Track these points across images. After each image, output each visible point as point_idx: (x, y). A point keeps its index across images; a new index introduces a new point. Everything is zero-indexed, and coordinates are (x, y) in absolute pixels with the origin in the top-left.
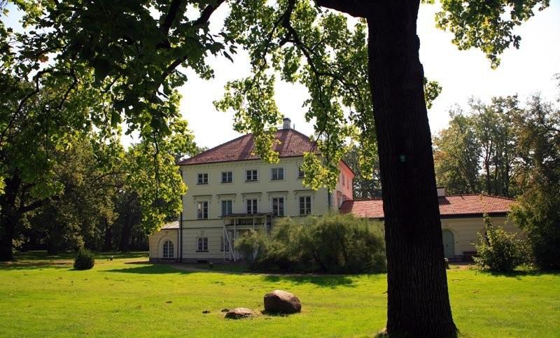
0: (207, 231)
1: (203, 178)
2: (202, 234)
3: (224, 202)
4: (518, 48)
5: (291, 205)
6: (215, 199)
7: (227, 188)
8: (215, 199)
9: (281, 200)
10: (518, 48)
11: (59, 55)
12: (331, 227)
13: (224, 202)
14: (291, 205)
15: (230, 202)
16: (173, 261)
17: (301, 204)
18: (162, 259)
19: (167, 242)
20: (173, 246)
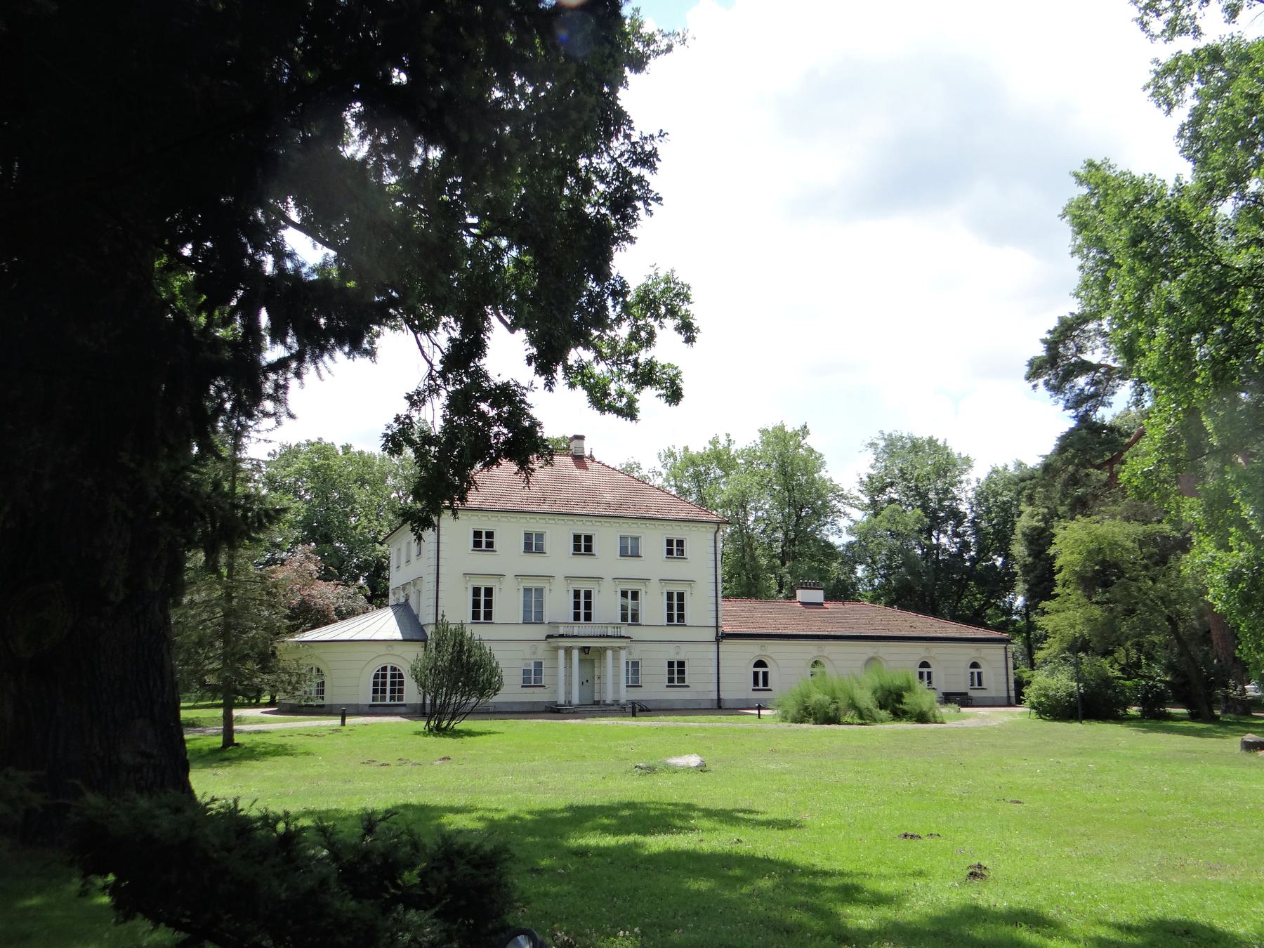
0: (684, 647)
1: (583, 543)
2: (534, 653)
3: (527, 591)
4: (690, 340)
5: (653, 607)
6: (559, 580)
7: (534, 564)
8: (559, 580)
9: (635, 595)
10: (690, 340)
11: (546, 359)
12: (494, 672)
13: (527, 591)
14: (653, 607)
15: (540, 591)
16: (403, 710)
17: (474, 612)
18: (371, 706)
19: (384, 669)
20: (401, 676)
